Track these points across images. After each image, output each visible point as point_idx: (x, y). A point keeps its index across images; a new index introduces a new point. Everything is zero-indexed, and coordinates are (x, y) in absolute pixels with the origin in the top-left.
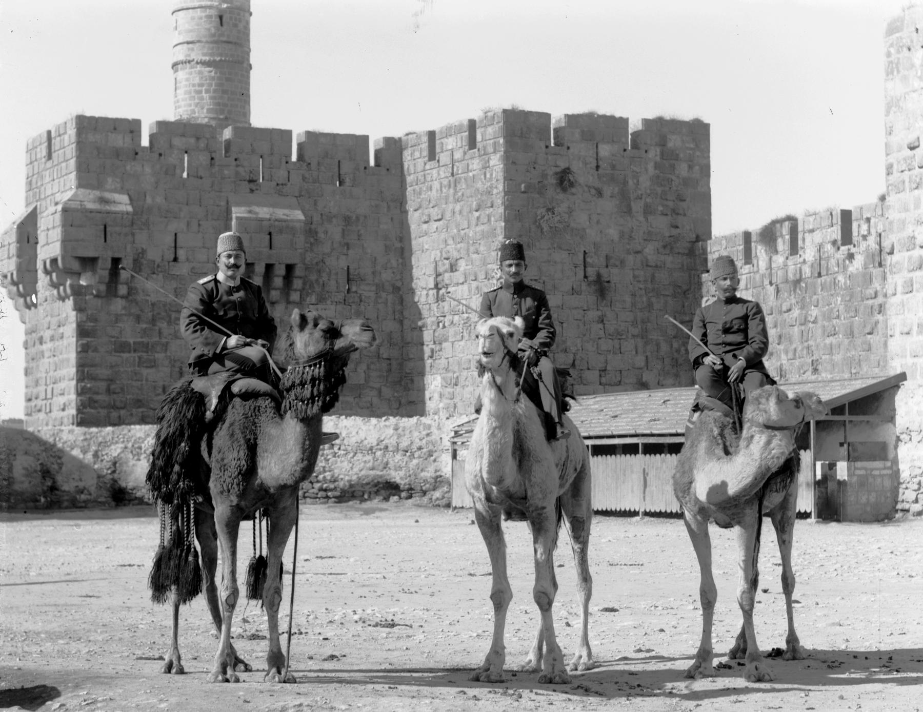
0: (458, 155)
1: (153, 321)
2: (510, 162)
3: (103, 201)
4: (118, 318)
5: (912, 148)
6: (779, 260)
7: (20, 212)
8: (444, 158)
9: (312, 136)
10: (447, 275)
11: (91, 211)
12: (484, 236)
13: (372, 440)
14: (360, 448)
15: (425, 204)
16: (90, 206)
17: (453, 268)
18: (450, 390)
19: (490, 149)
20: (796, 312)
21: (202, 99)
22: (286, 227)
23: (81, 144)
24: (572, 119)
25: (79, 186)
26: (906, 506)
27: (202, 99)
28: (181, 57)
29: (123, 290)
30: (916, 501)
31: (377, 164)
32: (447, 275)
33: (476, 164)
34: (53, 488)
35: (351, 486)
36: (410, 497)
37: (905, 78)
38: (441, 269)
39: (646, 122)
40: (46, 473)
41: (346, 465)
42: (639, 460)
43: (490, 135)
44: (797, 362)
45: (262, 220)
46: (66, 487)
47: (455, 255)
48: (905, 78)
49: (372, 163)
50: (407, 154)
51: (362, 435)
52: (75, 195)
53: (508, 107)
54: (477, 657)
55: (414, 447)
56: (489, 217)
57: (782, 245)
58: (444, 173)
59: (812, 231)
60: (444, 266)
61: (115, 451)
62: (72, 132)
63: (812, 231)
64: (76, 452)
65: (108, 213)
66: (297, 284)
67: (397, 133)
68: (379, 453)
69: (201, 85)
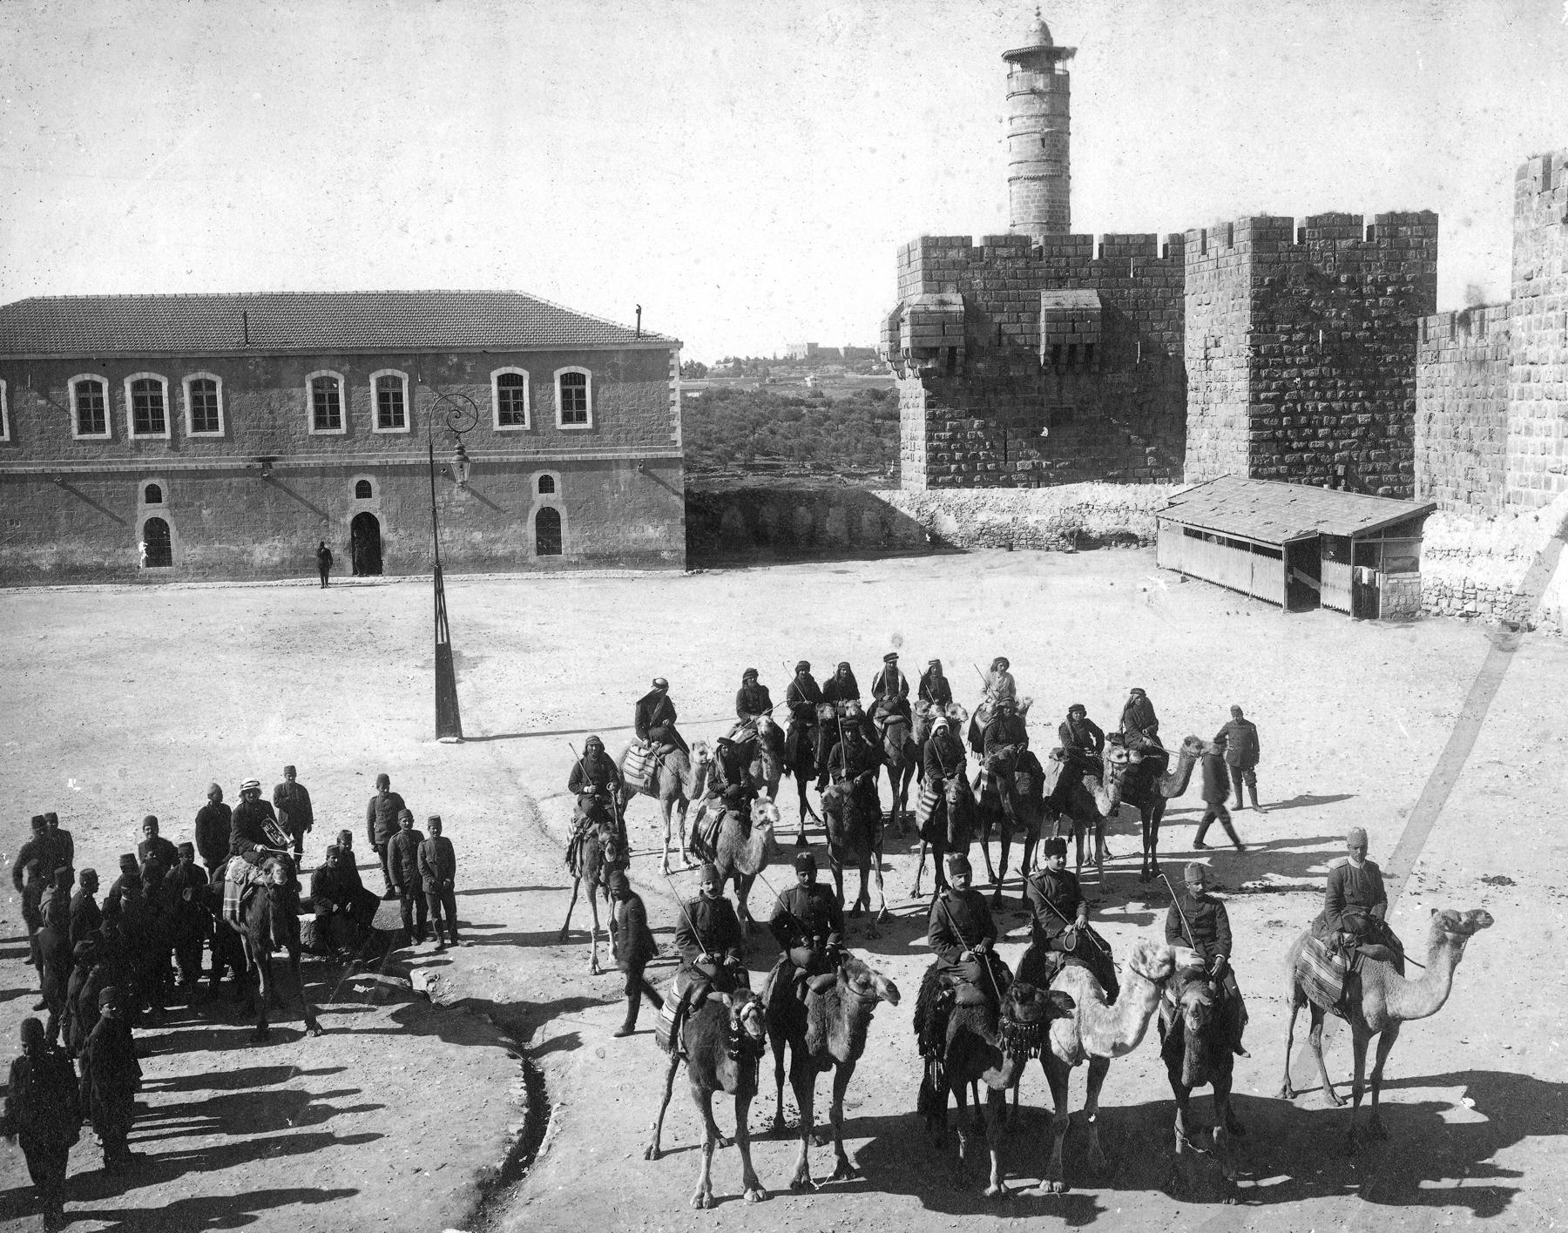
0: (1221, 252)
1: (984, 392)
2: (1257, 261)
3: (942, 303)
4: (956, 392)
5: (1529, 280)
6: (1472, 340)
7: (892, 307)
8: (1212, 254)
9: (1110, 239)
10: (1213, 349)
11: (933, 312)
12: (1238, 320)
13: (1116, 503)
14: (1107, 509)
15: (1199, 290)
16: (932, 308)
17: (1217, 345)
18: (1213, 441)
19: (1242, 250)
20: (1481, 388)
21: (1028, 208)
22: (1081, 315)
23: (926, 257)
24: (1313, 221)
25: (925, 292)
26: (1429, 608)
27: (1028, 208)
28: (1014, 175)
29: (959, 371)
30: (1437, 604)
31: (1165, 256)
32: (1213, 349)
33: (1233, 261)
34: (889, 535)
35: (1102, 536)
36: (1145, 546)
37: (1526, 218)
38: (1209, 345)
39: (1379, 217)
40: (884, 524)
41: (1097, 520)
42: (1249, 555)
43: (1243, 238)
44: (1480, 429)
45: (1066, 310)
46: (898, 535)
47: (1218, 334)
48: (1526, 218)
49: (1160, 255)
50: (1187, 247)
51: (1110, 498)
52: (922, 300)
53: (1256, 214)
54: (556, 926)
55: (1149, 507)
56: (1241, 305)
57: (1474, 328)
58: (1211, 265)
59: (1493, 321)
60: (1211, 343)
61: (932, 507)
62: (919, 245)
63: (1493, 321)
64: (904, 510)
65: (946, 312)
66: (1097, 358)
67: (1180, 230)
68: (1122, 512)
69: (1028, 197)
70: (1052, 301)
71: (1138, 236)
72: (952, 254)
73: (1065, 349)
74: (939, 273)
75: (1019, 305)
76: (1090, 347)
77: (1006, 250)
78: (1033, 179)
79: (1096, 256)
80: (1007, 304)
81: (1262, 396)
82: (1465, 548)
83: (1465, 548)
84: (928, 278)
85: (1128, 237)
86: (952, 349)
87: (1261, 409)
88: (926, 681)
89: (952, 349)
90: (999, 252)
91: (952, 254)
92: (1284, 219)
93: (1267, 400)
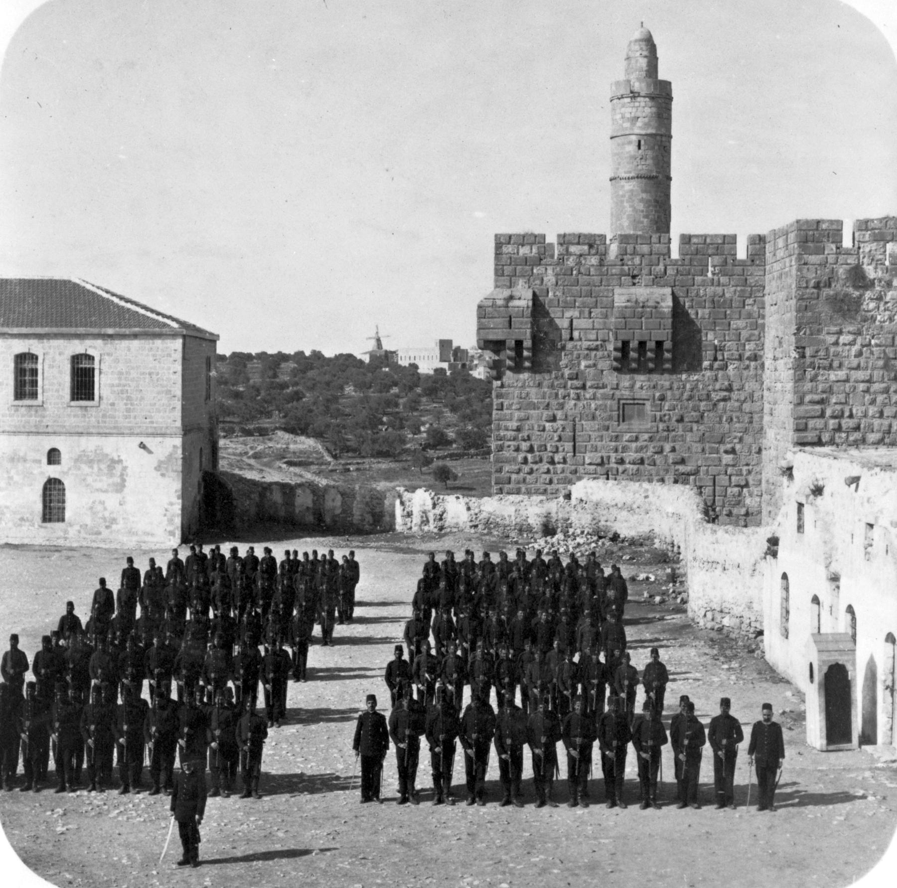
25: (496, 287)
70: (624, 298)
71: (716, 236)
72: (524, 251)
73: (651, 345)
74: (510, 268)
75: (590, 300)
76: (659, 344)
77: (579, 247)
78: (633, 178)
79: (675, 254)
80: (579, 300)
81: (808, 398)
82: (722, 562)
83: (722, 562)
84: (499, 272)
85: (705, 237)
86: (519, 344)
87: (807, 411)
88: (758, 728)
89: (519, 344)
90: (573, 249)
91: (524, 251)
92: (832, 222)
93: (813, 402)
